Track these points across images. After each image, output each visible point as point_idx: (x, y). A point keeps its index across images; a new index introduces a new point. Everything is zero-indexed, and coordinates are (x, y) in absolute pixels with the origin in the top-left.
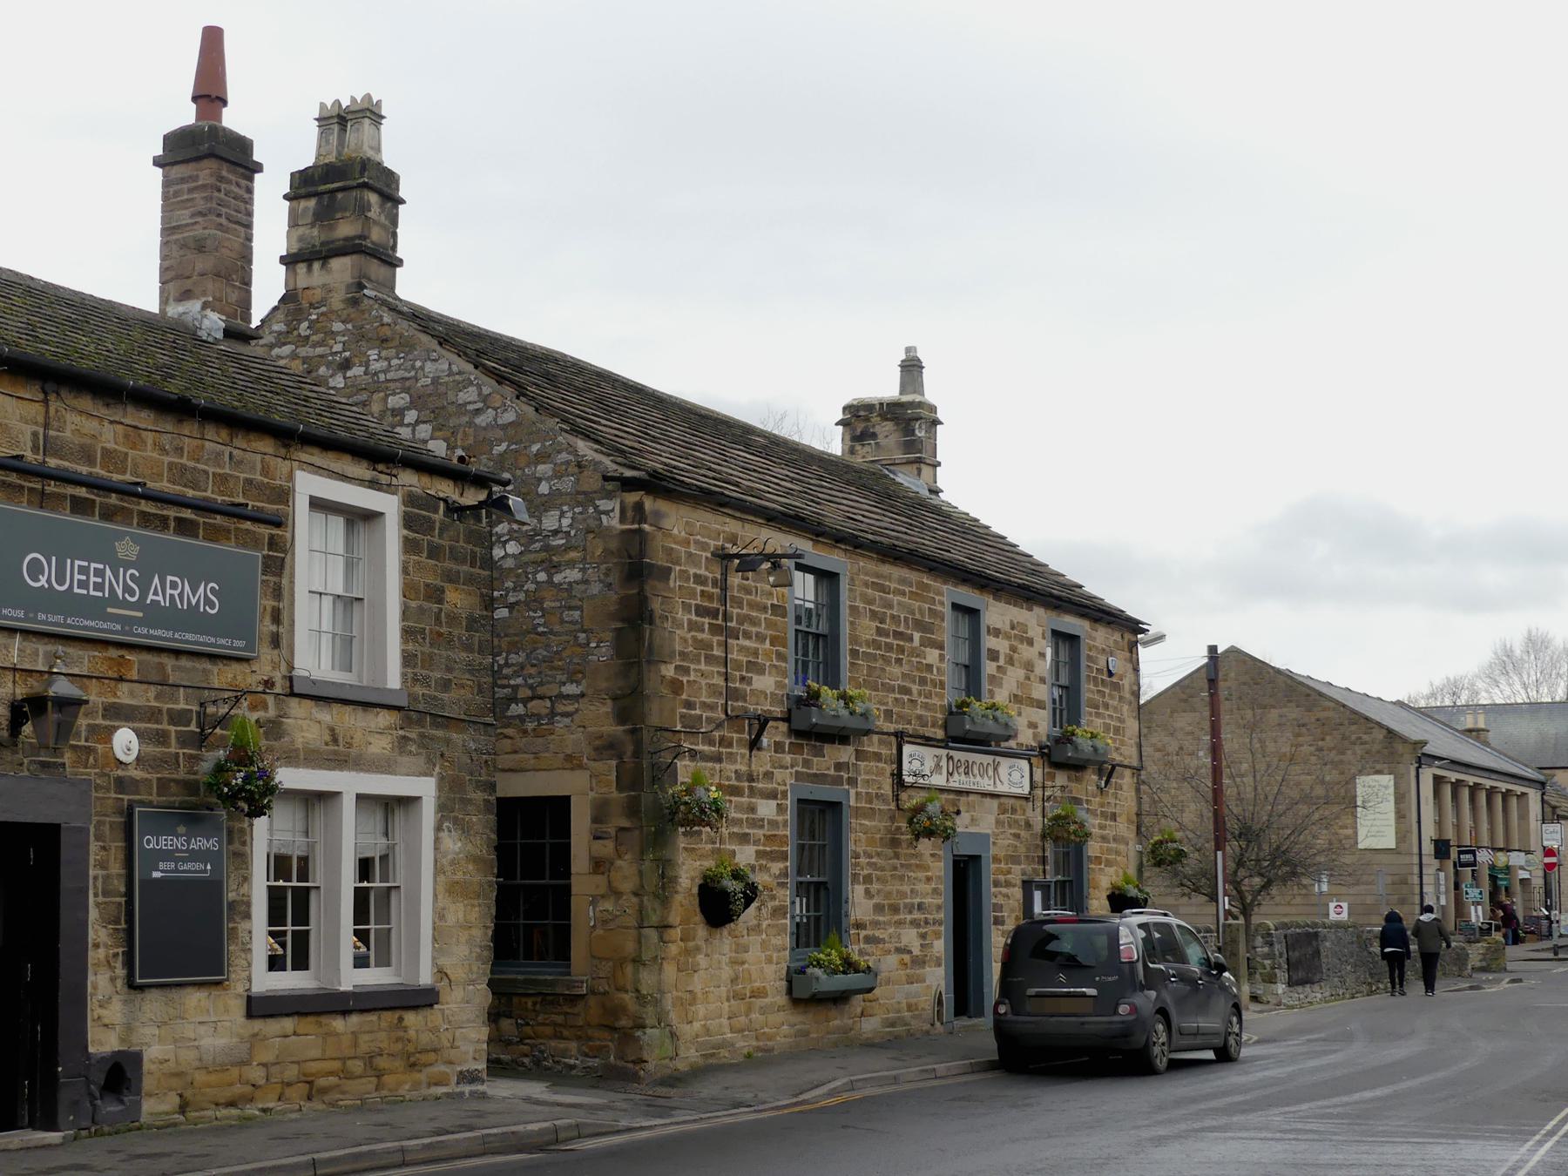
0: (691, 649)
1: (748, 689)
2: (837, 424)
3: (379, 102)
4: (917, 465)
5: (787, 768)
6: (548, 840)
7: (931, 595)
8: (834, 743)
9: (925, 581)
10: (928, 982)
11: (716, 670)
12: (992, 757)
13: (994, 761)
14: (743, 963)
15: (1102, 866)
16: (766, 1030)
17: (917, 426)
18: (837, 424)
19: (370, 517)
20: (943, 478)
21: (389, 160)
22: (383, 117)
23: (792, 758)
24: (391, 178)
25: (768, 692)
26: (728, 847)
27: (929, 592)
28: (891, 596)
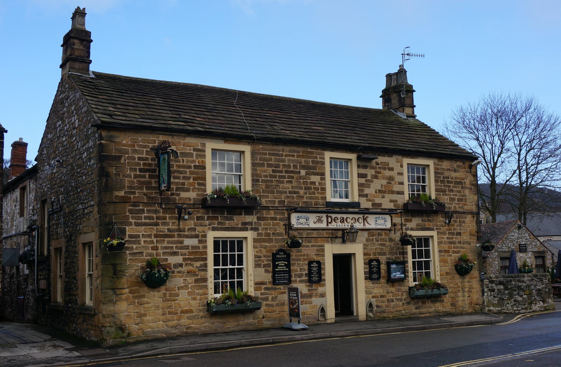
0: (136, 185)
1: (177, 198)
2: (380, 97)
3: (84, 9)
4: (402, 108)
5: (207, 226)
6: (236, 253)
7: (314, 155)
8: (241, 214)
9: (309, 150)
10: (314, 304)
11: (154, 192)
12: (363, 215)
13: (363, 217)
14: (176, 300)
15: (451, 254)
16: (192, 325)
17: (402, 93)
18: (380, 97)
19: (243, 152)
20: (417, 111)
21: (88, 28)
22: (86, 14)
23: (209, 222)
24: (89, 34)
25: (192, 198)
26: (162, 257)
27: (314, 154)
28: (284, 157)
